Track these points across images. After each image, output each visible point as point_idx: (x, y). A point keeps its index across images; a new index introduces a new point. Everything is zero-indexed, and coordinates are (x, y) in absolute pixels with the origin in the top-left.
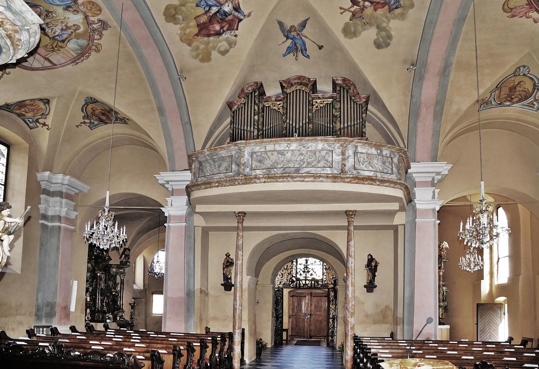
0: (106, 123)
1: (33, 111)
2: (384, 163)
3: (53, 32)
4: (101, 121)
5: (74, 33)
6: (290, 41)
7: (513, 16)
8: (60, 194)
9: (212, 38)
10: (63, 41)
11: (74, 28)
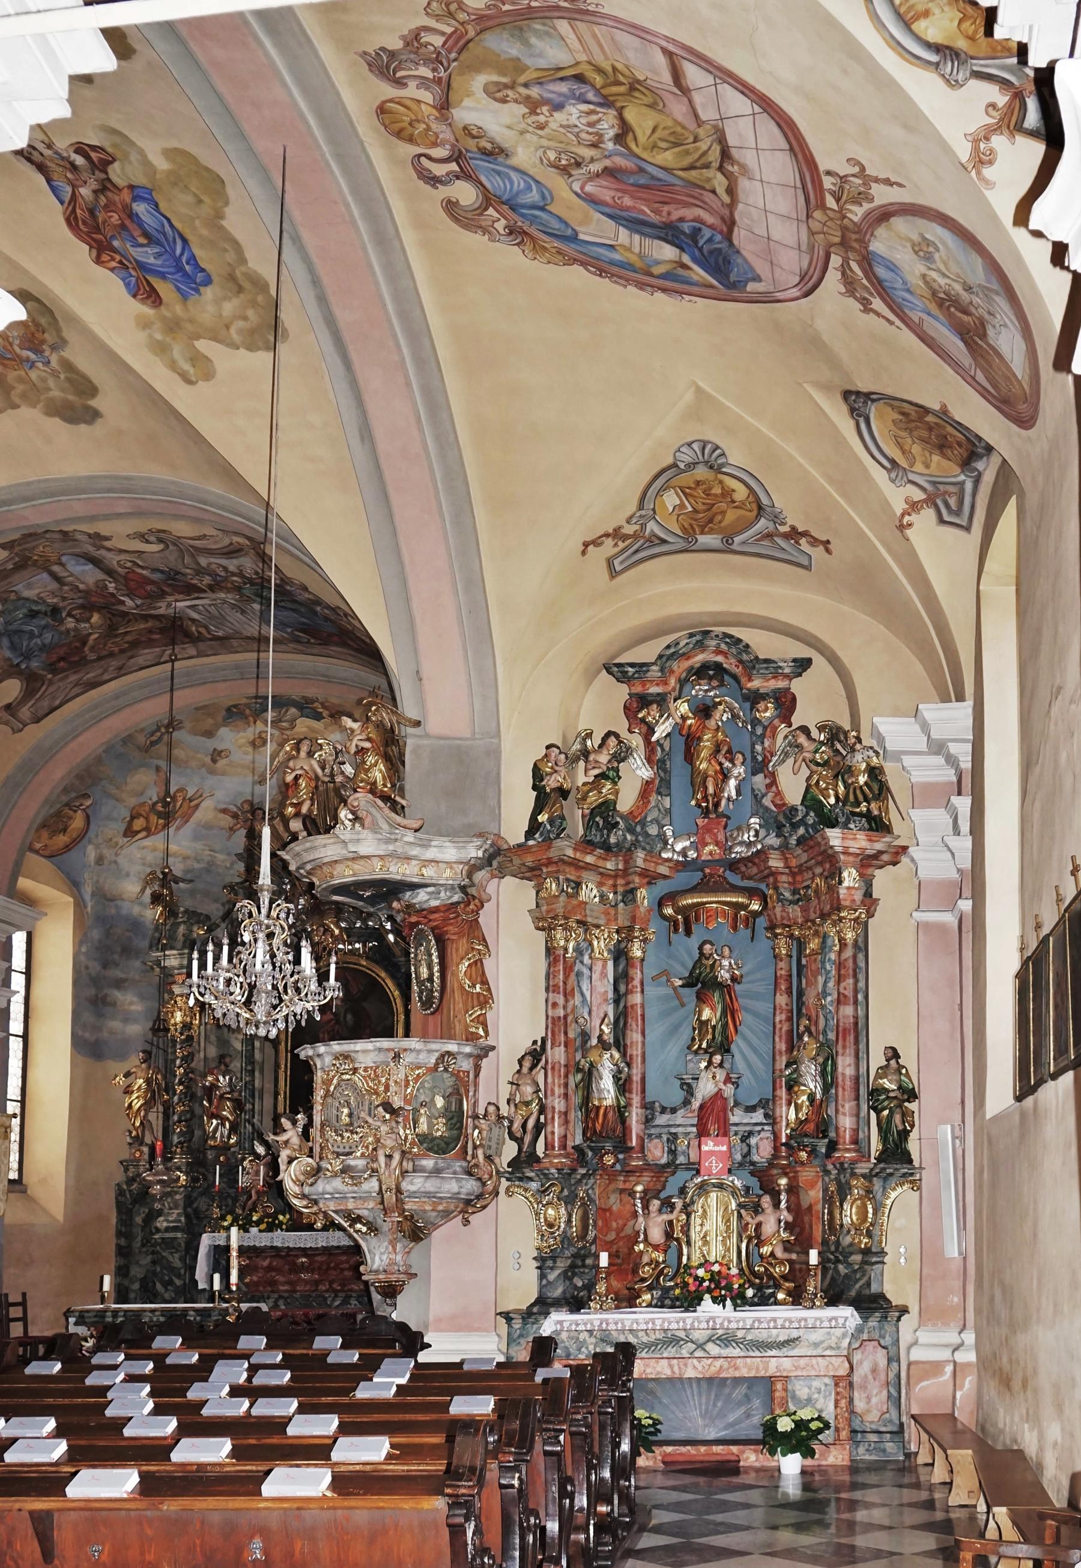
3: (594, 118)
5: (522, 79)
10: (580, 78)
11: (510, 92)
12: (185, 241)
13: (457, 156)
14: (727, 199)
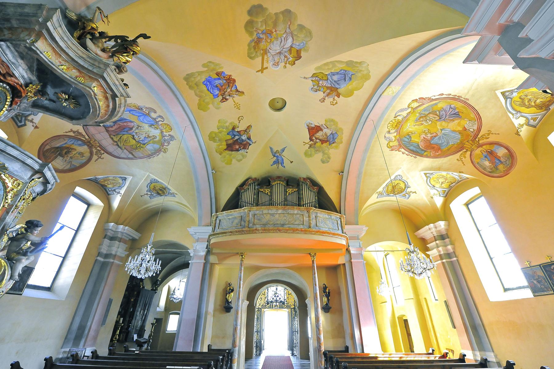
0: (161, 196)
1: (113, 183)
2: (333, 223)
4: (158, 194)
6: (275, 158)
7: (392, 150)
8: (120, 240)
9: (233, 152)
10: (144, 144)
12: (208, 90)
13: (157, 122)
14: (112, 136)
